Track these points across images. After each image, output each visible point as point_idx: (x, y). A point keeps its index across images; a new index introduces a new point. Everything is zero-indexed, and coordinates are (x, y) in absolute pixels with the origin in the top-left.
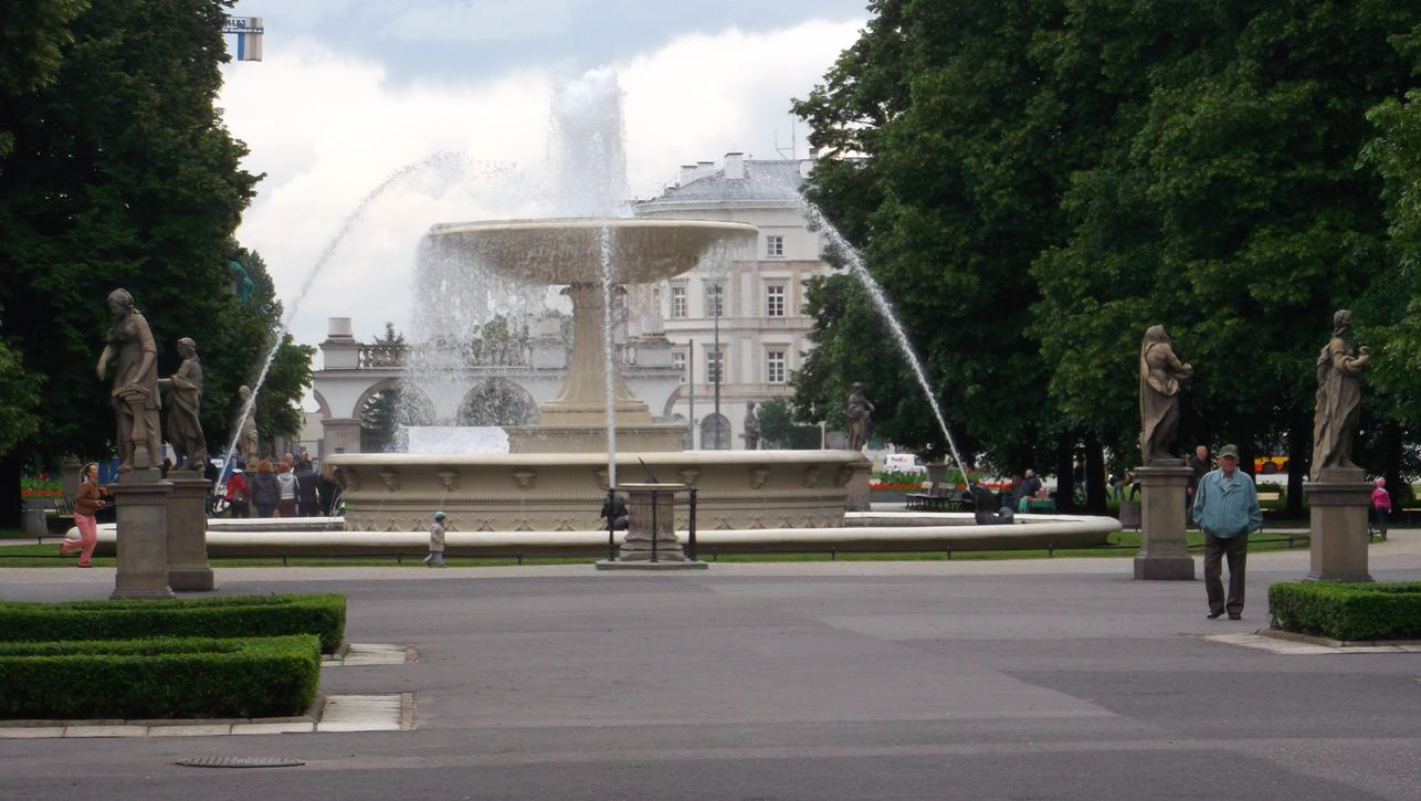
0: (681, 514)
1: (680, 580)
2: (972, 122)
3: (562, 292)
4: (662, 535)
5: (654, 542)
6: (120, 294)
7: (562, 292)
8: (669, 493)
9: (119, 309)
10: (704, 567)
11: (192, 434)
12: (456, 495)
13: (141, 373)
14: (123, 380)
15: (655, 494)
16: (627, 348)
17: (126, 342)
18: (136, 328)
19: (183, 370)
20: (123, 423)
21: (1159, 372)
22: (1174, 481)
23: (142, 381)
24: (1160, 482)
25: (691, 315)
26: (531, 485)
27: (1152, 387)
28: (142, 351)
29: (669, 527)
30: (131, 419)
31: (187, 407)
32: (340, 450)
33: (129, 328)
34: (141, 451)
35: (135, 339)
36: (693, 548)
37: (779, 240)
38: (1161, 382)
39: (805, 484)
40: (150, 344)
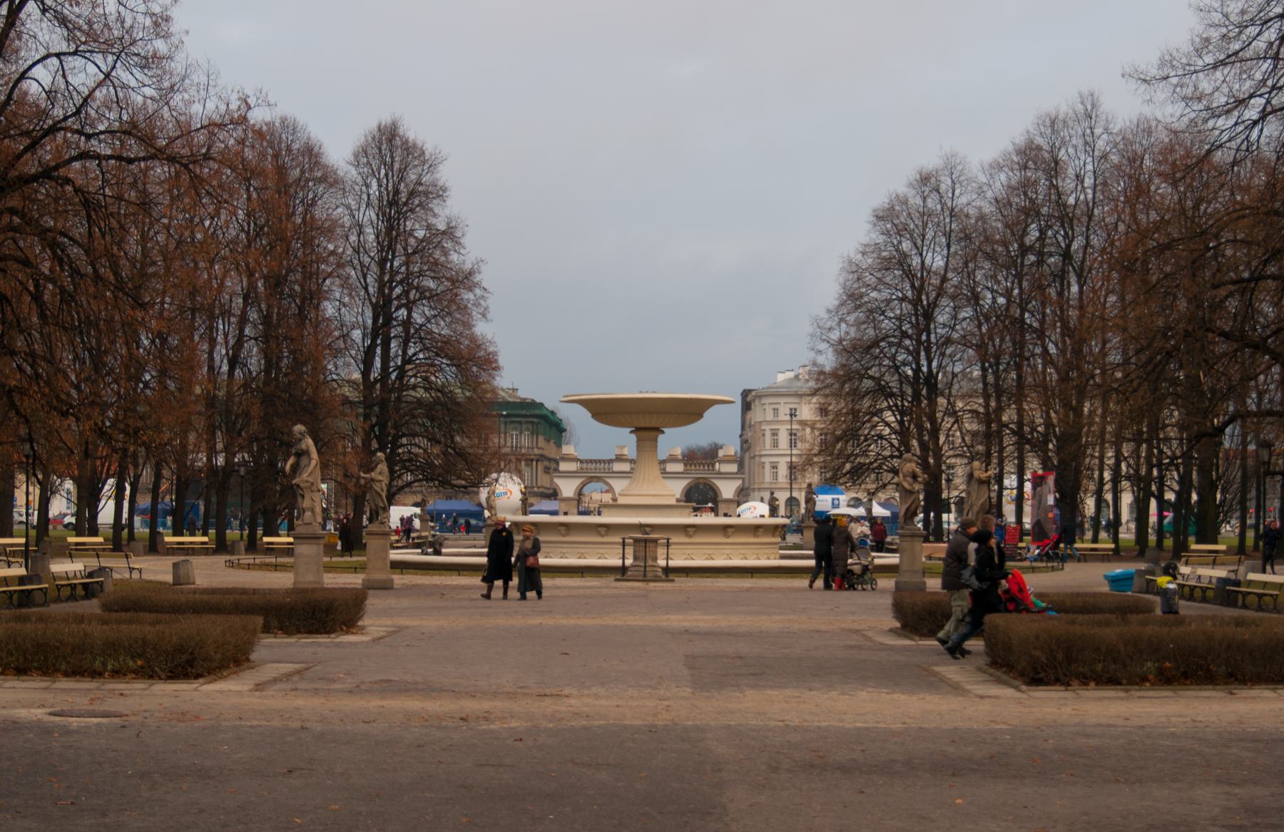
0: (661, 552)
1: (439, 592)
2: (385, 304)
3: (631, 432)
4: (650, 563)
5: (645, 567)
6: (299, 428)
7: (631, 432)
8: (655, 541)
9: (299, 436)
10: (673, 581)
11: (381, 505)
12: (567, 539)
13: (309, 470)
14: (300, 474)
15: (646, 541)
16: (537, 461)
17: (302, 454)
18: (307, 446)
19: (378, 470)
20: (299, 499)
21: (909, 479)
22: (916, 539)
23: (309, 475)
24: (908, 539)
25: (780, 447)
26: (607, 535)
27: (521, 478)
28: (310, 459)
29: (655, 559)
30: (303, 496)
31: (379, 490)
32: (566, 514)
33: (304, 446)
34: (308, 514)
35: (306, 453)
36: (668, 571)
37: (795, 409)
38: (910, 485)
39: (755, 536)
40: (314, 455)
